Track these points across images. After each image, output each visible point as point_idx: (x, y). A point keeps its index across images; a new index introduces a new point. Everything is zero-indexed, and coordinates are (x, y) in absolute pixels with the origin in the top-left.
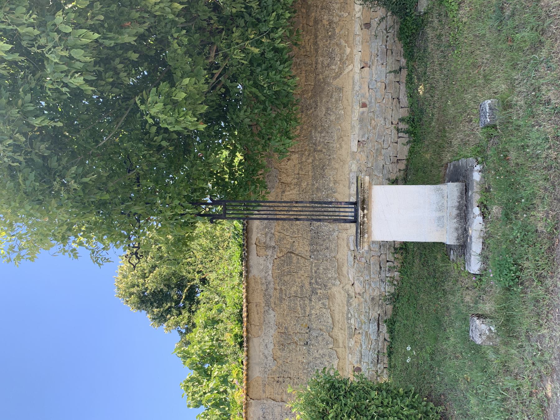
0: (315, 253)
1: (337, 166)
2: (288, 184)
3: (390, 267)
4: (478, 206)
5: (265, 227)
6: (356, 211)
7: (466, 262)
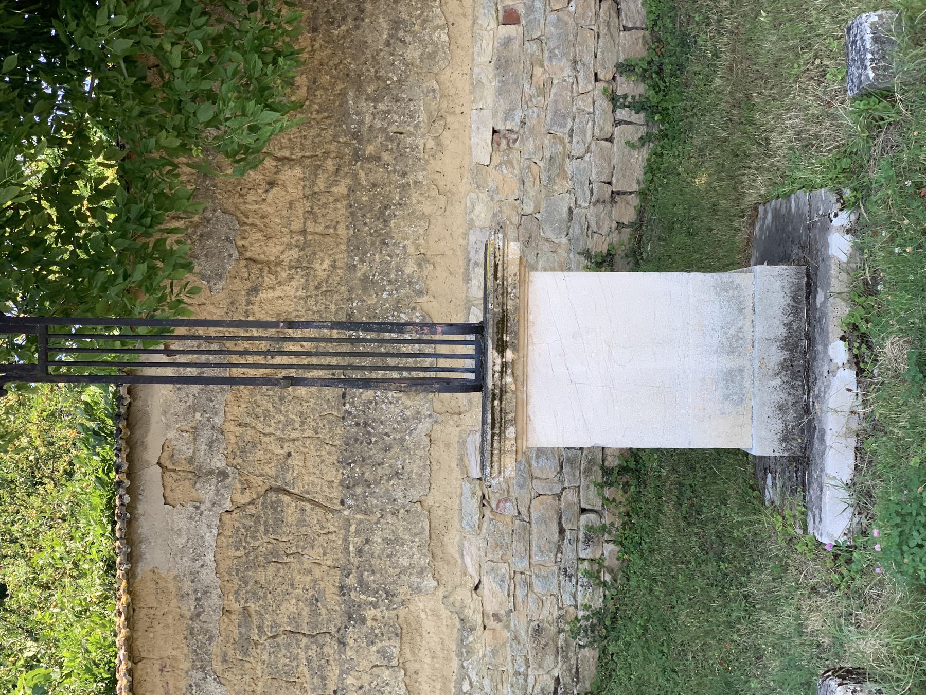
0: (359, 490)
1: (427, 208)
2: (271, 266)
3: (590, 528)
4: (843, 338)
5: (194, 408)
6: (481, 353)
7: (808, 508)
